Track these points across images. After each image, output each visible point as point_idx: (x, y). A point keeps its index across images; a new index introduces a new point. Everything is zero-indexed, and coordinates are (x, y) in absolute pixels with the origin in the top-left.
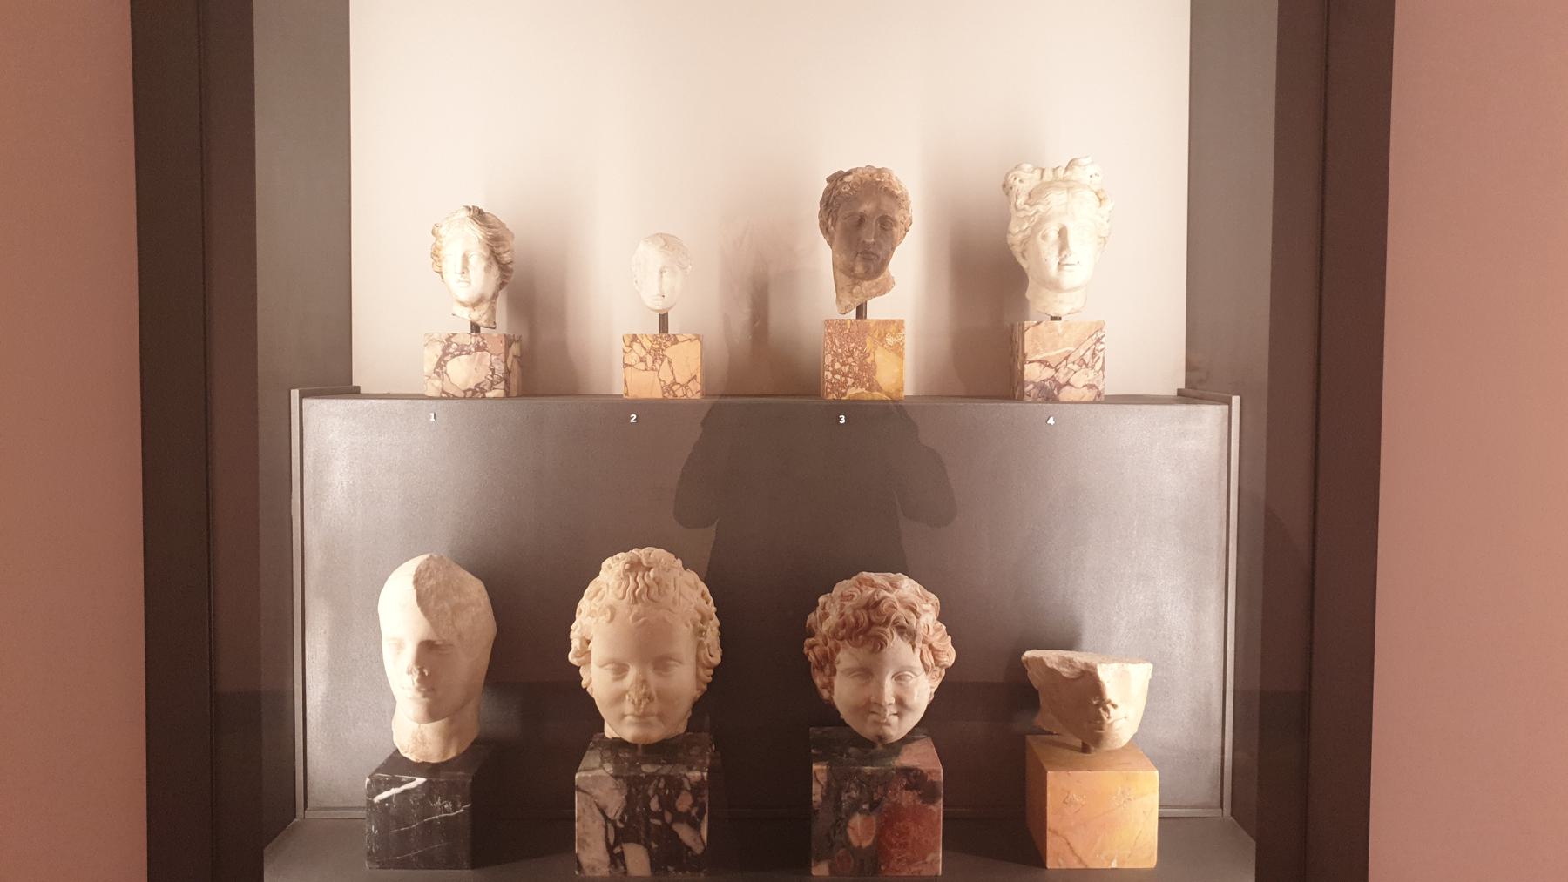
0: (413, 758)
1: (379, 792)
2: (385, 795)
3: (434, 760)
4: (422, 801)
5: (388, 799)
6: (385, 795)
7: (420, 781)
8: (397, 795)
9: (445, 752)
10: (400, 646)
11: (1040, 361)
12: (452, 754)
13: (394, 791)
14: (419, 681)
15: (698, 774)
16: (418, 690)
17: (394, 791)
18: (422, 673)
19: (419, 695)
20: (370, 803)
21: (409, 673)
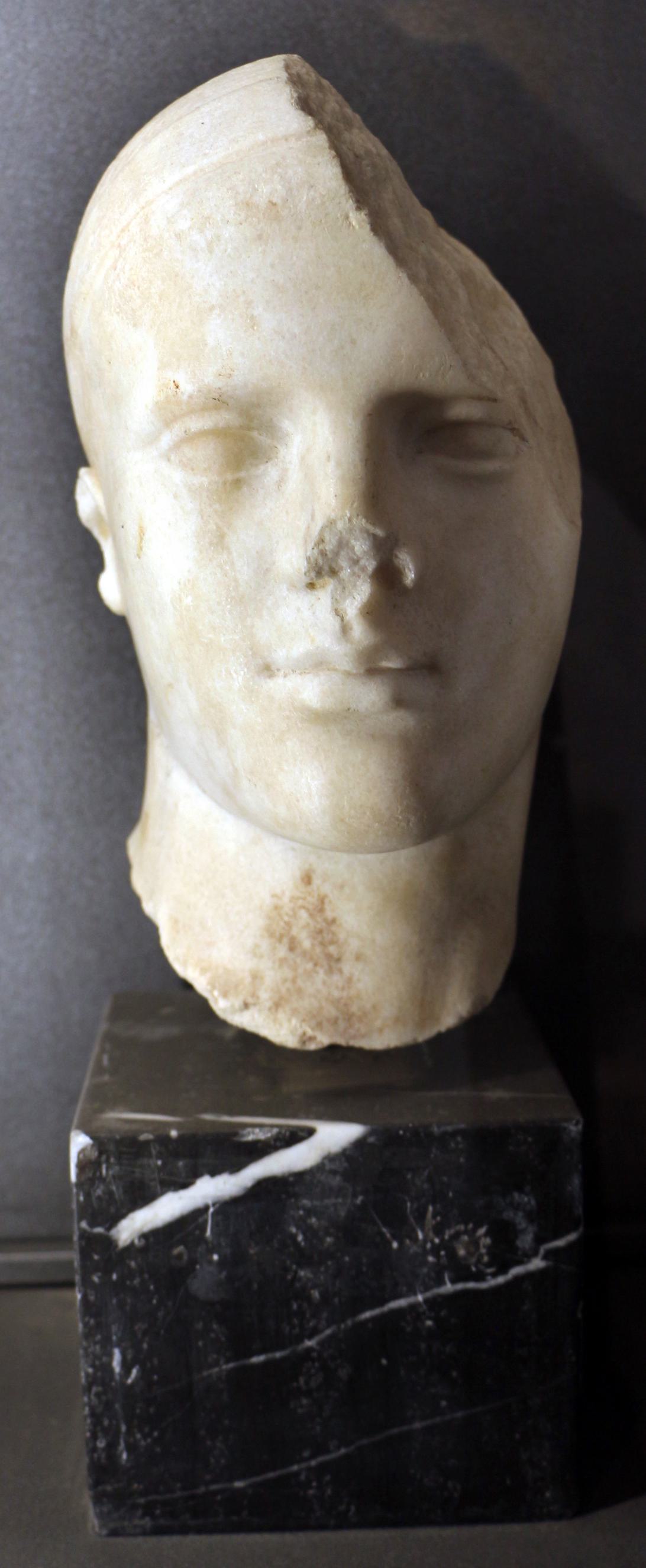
0: (283, 1032)
1: (142, 1197)
2: (168, 1207)
3: (381, 1037)
4: (350, 1231)
5: (184, 1227)
6: (168, 1207)
7: (334, 1136)
8: (227, 1207)
9: (424, 998)
10: (239, 437)
11: (313, 510)
12: (454, 1009)
13: (210, 1189)
14: (373, 613)
15: (302, 1273)
16: (370, 667)
17: (210, 1189)
18: (386, 575)
19: (371, 696)
20: (100, 1250)
21: (322, 569)
